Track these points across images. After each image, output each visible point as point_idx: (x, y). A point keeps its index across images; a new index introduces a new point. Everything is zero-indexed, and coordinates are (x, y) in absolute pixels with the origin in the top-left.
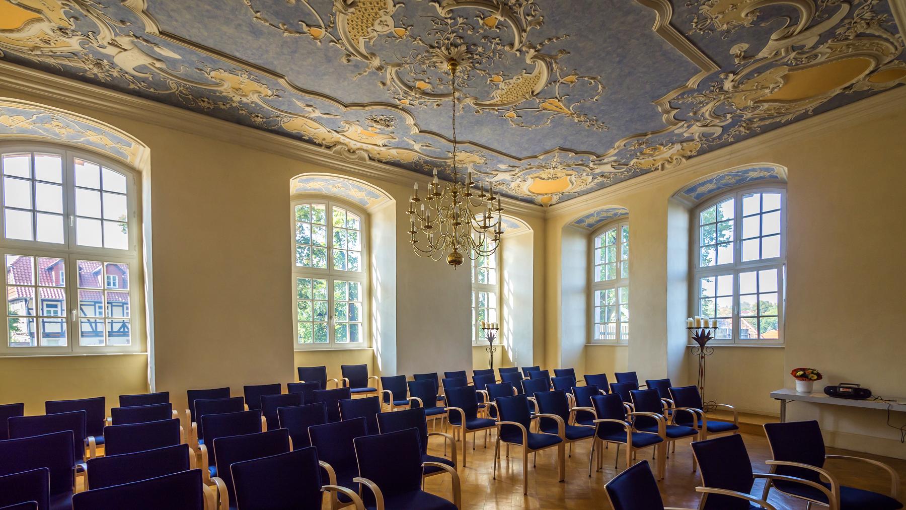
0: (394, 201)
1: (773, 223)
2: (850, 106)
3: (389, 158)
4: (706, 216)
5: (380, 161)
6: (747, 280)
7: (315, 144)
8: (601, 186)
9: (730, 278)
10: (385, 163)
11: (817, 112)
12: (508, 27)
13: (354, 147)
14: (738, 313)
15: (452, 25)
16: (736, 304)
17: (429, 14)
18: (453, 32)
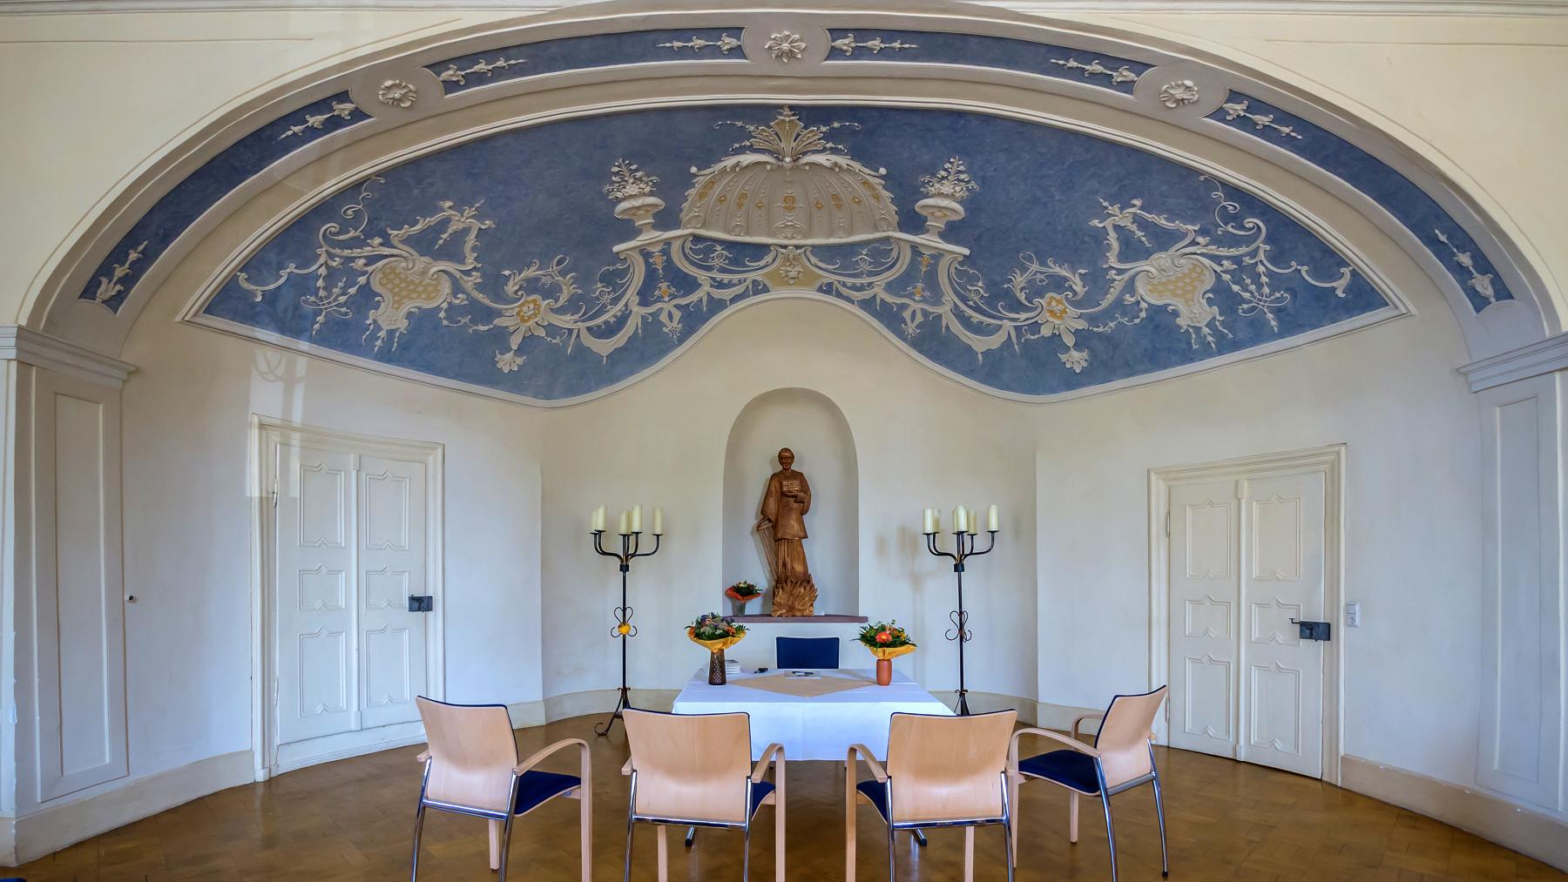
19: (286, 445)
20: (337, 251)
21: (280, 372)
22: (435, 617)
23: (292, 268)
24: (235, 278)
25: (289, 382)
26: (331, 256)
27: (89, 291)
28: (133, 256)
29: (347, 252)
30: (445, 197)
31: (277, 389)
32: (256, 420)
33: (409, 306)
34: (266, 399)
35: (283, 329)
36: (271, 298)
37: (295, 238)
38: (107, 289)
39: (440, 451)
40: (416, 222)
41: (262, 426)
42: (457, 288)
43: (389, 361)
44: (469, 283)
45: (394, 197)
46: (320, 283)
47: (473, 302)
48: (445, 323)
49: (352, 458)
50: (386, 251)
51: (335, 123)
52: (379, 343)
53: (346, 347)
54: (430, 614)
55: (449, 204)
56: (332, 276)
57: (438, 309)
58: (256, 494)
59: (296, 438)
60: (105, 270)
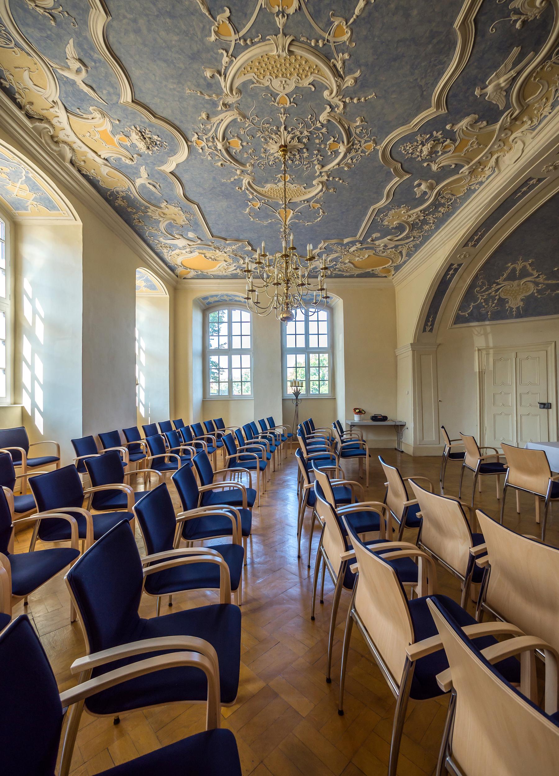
0: (80, 223)
1: (247, 329)
2: (373, 278)
3: (92, 173)
4: (212, 316)
5: (79, 171)
6: (236, 359)
7: (14, 100)
8: (234, 277)
9: (226, 358)
10: (83, 175)
11: (359, 276)
12: (336, 157)
13: (62, 136)
14: (232, 379)
15: (318, 129)
16: (230, 374)
17: (315, 110)
18: (310, 132)
19: (488, 354)
20: (484, 294)
21: (482, 332)
22: (553, 412)
23: (472, 304)
24: (458, 314)
25: (486, 335)
26: (483, 296)
27: (424, 330)
28: (431, 319)
29: (487, 293)
30: (507, 263)
31: (482, 337)
32: (477, 349)
33: (522, 296)
34: (479, 342)
35: (478, 320)
36: (471, 314)
37: (469, 295)
38: (428, 329)
39: (553, 344)
40: (504, 275)
41: (479, 350)
42: (536, 284)
43: (522, 317)
44: (541, 279)
45: (490, 272)
46: (483, 304)
47: (547, 285)
48: (539, 296)
49: (514, 355)
50: (499, 286)
51: (456, 270)
52: (514, 313)
53: (503, 318)
54: (550, 410)
55: (510, 264)
56: (486, 301)
57: (533, 293)
58: (478, 371)
59: (491, 351)
60: (426, 324)
